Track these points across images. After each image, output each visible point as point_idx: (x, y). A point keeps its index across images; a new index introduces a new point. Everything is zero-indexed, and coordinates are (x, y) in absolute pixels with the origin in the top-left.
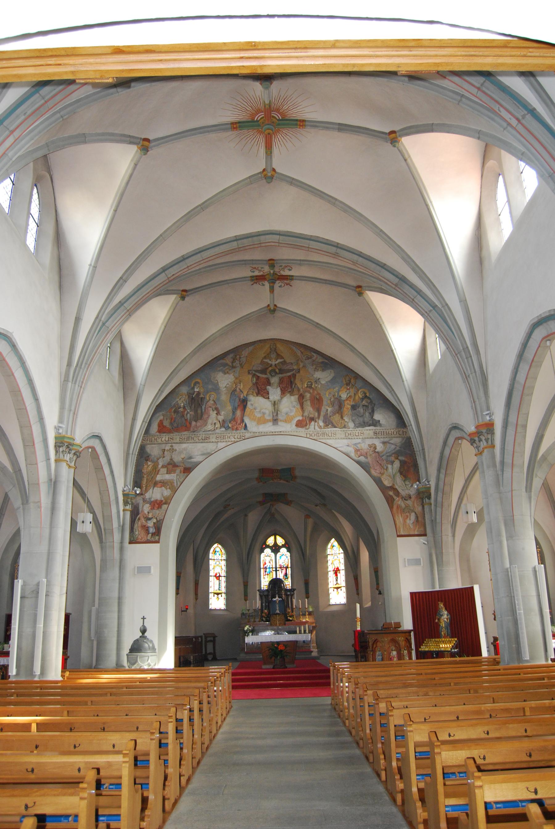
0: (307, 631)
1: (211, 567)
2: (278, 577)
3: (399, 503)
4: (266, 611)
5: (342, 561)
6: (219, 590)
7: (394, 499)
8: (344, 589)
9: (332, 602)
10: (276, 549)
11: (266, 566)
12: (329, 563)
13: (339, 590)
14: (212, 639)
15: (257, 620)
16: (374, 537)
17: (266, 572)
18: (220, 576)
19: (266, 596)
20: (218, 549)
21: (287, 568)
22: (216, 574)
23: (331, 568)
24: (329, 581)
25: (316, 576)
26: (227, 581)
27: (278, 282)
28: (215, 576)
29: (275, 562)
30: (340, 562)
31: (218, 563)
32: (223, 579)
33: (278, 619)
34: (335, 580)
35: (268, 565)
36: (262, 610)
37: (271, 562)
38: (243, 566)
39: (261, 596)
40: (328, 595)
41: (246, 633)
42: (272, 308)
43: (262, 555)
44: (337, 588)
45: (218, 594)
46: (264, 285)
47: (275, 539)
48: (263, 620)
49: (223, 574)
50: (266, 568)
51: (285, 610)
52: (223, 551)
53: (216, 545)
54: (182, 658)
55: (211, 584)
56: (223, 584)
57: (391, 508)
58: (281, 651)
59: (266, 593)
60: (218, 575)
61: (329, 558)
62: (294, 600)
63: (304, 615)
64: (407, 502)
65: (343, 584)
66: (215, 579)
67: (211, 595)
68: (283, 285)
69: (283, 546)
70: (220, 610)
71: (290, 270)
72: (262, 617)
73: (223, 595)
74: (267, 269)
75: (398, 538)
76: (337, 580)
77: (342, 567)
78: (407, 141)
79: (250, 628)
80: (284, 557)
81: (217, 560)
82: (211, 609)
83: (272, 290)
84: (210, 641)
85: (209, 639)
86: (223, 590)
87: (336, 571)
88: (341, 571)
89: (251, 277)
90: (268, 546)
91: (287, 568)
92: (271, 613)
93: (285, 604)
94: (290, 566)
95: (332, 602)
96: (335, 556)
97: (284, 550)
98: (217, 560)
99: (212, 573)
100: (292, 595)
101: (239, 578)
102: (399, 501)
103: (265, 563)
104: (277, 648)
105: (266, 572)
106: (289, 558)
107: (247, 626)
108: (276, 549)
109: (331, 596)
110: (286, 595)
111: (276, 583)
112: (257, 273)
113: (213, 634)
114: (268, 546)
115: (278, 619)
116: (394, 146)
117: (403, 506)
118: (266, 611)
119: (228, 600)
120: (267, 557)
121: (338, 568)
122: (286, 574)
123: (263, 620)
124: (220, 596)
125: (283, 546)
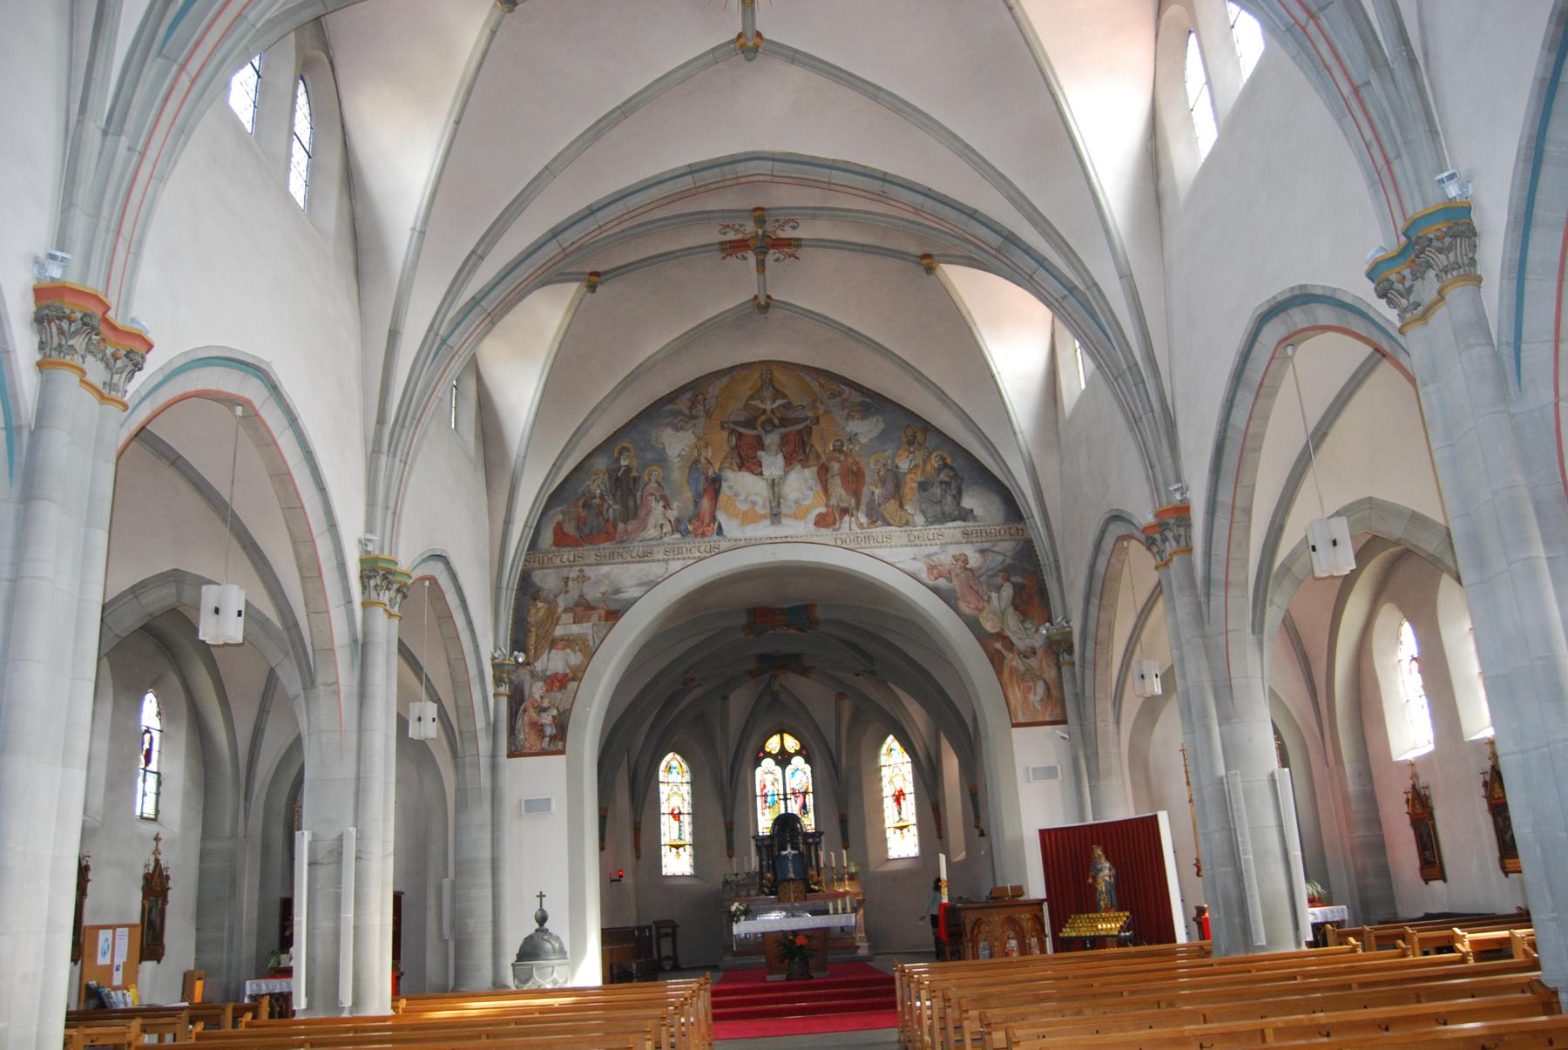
1: (663, 797)
8: (914, 830)
9: (892, 854)
10: (783, 759)
12: (885, 782)
14: (669, 930)
19: (769, 847)
21: (805, 793)
29: (782, 784)
32: (686, 819)
35: (769, 789)
36: (761, 874)
39: (759, 848)
41: (733, 917)
43: (759, 771)
44: (901, 828)
45: (677, 847)
49: (686, 809)
51: (806, 873)
55: (664, 829)
62: (821, 854)
67: (665, 850)
69: (797, 753)
70: (683, 876)
71: (794, 228)
72: (762, 886)
74: (750, 228)
77: (909, 788)
80: (799, 774)
81: (675, 783)
84: (666, 935)
85: (663, 931)
86: (688, 838)
87: (899, 797)
89: (721, 243)
90: (769, 755)
91: (805, 793)
93: (805, 861)
95: (892, 854)
96: (895, 767)
97: (798, 761)
99: (665, 808)
100: (817, 845)
108: (783, 759)
109: (890, 844)
111: (786, 823)
112: (731, 236)
114: (769, 755)
117: (1022, 668)
120: (766, 775)
122: (804, 806)
125: (797, 753)
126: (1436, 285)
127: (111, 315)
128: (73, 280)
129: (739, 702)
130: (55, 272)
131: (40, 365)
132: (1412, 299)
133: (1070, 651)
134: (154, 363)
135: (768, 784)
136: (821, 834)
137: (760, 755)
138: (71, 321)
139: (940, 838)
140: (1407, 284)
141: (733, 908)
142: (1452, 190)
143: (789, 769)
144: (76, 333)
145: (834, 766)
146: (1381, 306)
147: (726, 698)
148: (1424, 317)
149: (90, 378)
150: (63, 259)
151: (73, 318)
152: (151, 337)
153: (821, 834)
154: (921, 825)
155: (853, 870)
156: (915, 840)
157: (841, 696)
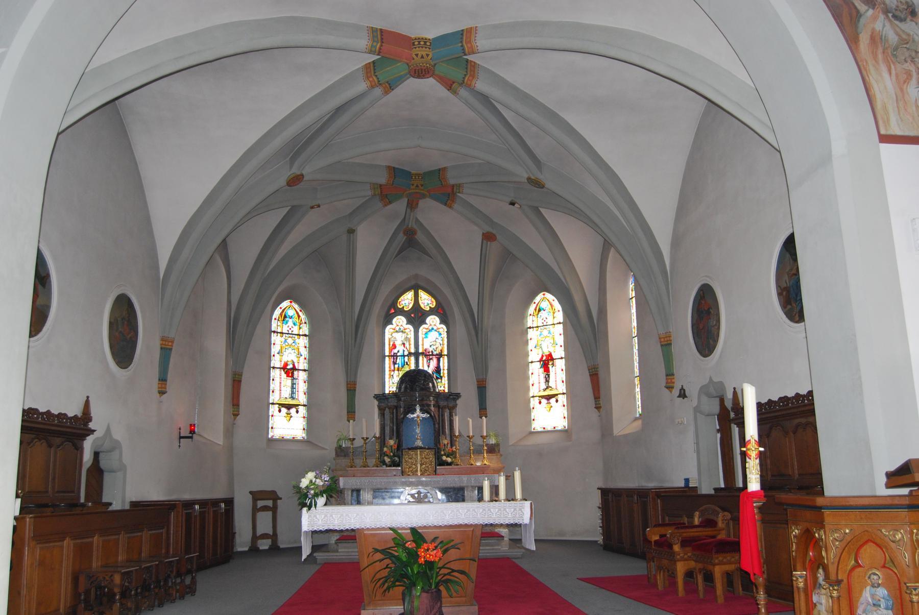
0: (519, 495)
1: (275, 350)
2: (421, 367)
3: (878, 26)
4: (392, 442)
5: (560, 340)
6: (293, 398)
7: (859, 15)
8: (563, 399)
9: (537, 426)
10: (417, 317)
11: (395, 351)
12: (531, 345)
13: (553, 400)
14: (270, 503)
15: (372, 461)
16: (664, 262)
17: (395, 363)
18: (294, 369)
19: (394, 408)
20: (291, 312)
21: (440, 356)
22: (286, 364)
23: (534, 356)
24: (531, 382)
25: (503, 371)
26: (310, 382)
28: (284, 368)
29: (414, 341)
30: (555, 344)
31: (290, 341)
32: (302, 376)
33: (419, 459)
34: (543, 380)
35: (400, 349)
36: (382, 440)
37: (407, 345)
38: (346, 342)
39: (382, 410)
40: (528, 410)
41: (304, 500)
43: (389, 329)
44: (548, 398)
45: (289, 407)
47: (416, 296)
48: (384, 463)
49: (302, 364)
50: (395, 356)
51: (437, 441)
52: (303, 316)
53: (285, 304)
54: (82, 579)
55: (274, 385)
56: (302, 387)
57: (852, 40)
58: (430, 564)
59: (393, 402)
60: (290, 366)
61: (531, 334)
62: (457, 420)
63: (478, 452)
64: (902, 25)
65: (562, 388)
66: (284, 375)
67: (273, 410)
69: (432, 312)
70: (294, 440)
72: (383, 454)
73: (301, 409)
75: (885, 148)
76: (547, 381)
77: (559, 353)
79: (319, 482)
80: (433, 335)
81: (289, 338)
82: (272, 440)
84: (265, 508)
85: (260, 504)
86: (302, 399)
87: (547, 362)
88: (557, 362)
90: (401, 312)
91: (440, 356)
92: (404, 446)
93: (438, 427)
94: (445, 352)
95: (537, 426)
96: (545, 327)
97: (433, 321)
98: (289, 338)
99: (276, 362)
100: (452, 409)
101: (335, 374)
102: (875, 18)
103: (394, 346)
104: (413, 555)
105: (395, 363)
106: (445, 335)
107: (311, 475)
108: (417, 317)
109: (534, 414)
110: (437, 406)
111: (415, 381)
113: (274, 492)
114: (401, 312)
115: (419, 459)
117: (892, 38)
118: (392, 442)
119: (311, 421)
120: (398, 333)
121: (550, 355)
122: (438, 370)
123: (384, 463)
124: (293, 411)
125: (432, 312)
129: (371, 242)
135: (398, 343)
136: (458, 396)
137: (391, 311)
139: (598, 408)
141: (304, 483)
143: (422, 330)
145: (476, 328)
147: (351, 231)
153: (458, 396)
154: (570, 393)
155: (493, 441)
156: (565, 412)
157: (488, 237)
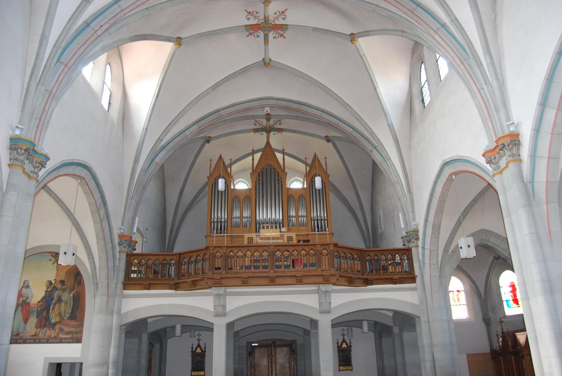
27: (272, 32)
42: (267, 62)
46: (258, 36)
47: (268, 137)
68: (277, 36)
71: (280, 124)
74: (264, 122)
78: (361, 42)
83: (266, 41)
89: (246, 26)
112: (253, 22)
116: (353, 44)
126: (506, 162)
127: (36, 148)
128: (24, 136)
130: (18, 132)
131: (9, 165)
132: (498, 165)
133: (417, 239)
134: (50, 165)
138: (21, 149)
140: (496, 160)
142: (512, 129)
144: (22, 154)
146: (488, 166)
148: (501, 172)
149: (26, 170)
150: (21, 128)
151: (24, 151)
152: (49, 155)
